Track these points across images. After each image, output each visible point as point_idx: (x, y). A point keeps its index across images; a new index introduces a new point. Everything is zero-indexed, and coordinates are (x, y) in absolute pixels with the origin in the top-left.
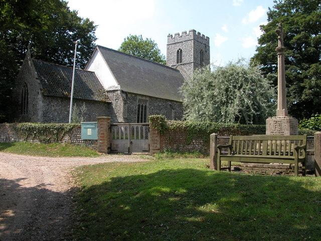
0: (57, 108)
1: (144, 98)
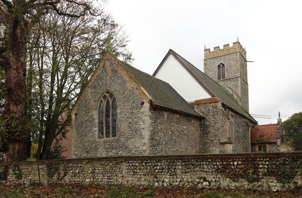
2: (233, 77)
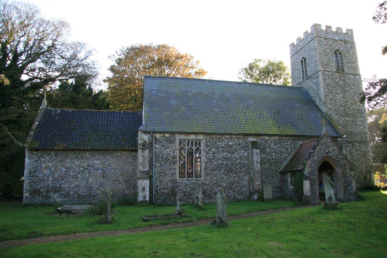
0: (50, 164)
1: (192, 137)
2: (315, 72)
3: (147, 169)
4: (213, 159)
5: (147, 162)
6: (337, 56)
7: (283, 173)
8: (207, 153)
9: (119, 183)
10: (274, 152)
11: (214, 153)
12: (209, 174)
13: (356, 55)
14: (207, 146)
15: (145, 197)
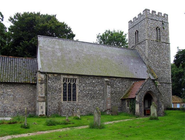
1: (71, 77)
3: (44, 95)
4: (83, 90)
5: (44, 91)
6: (157, 31)
7: (123, 100)
8: (80, 86)
9: (25, 104)
10: (118, 87)
11: (84, 87)
12: (81, 99)
13: (168, 31)
14: (80, 82)
15: (43, 112)
